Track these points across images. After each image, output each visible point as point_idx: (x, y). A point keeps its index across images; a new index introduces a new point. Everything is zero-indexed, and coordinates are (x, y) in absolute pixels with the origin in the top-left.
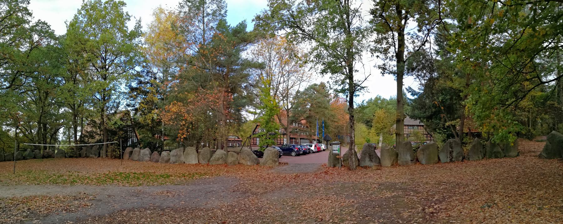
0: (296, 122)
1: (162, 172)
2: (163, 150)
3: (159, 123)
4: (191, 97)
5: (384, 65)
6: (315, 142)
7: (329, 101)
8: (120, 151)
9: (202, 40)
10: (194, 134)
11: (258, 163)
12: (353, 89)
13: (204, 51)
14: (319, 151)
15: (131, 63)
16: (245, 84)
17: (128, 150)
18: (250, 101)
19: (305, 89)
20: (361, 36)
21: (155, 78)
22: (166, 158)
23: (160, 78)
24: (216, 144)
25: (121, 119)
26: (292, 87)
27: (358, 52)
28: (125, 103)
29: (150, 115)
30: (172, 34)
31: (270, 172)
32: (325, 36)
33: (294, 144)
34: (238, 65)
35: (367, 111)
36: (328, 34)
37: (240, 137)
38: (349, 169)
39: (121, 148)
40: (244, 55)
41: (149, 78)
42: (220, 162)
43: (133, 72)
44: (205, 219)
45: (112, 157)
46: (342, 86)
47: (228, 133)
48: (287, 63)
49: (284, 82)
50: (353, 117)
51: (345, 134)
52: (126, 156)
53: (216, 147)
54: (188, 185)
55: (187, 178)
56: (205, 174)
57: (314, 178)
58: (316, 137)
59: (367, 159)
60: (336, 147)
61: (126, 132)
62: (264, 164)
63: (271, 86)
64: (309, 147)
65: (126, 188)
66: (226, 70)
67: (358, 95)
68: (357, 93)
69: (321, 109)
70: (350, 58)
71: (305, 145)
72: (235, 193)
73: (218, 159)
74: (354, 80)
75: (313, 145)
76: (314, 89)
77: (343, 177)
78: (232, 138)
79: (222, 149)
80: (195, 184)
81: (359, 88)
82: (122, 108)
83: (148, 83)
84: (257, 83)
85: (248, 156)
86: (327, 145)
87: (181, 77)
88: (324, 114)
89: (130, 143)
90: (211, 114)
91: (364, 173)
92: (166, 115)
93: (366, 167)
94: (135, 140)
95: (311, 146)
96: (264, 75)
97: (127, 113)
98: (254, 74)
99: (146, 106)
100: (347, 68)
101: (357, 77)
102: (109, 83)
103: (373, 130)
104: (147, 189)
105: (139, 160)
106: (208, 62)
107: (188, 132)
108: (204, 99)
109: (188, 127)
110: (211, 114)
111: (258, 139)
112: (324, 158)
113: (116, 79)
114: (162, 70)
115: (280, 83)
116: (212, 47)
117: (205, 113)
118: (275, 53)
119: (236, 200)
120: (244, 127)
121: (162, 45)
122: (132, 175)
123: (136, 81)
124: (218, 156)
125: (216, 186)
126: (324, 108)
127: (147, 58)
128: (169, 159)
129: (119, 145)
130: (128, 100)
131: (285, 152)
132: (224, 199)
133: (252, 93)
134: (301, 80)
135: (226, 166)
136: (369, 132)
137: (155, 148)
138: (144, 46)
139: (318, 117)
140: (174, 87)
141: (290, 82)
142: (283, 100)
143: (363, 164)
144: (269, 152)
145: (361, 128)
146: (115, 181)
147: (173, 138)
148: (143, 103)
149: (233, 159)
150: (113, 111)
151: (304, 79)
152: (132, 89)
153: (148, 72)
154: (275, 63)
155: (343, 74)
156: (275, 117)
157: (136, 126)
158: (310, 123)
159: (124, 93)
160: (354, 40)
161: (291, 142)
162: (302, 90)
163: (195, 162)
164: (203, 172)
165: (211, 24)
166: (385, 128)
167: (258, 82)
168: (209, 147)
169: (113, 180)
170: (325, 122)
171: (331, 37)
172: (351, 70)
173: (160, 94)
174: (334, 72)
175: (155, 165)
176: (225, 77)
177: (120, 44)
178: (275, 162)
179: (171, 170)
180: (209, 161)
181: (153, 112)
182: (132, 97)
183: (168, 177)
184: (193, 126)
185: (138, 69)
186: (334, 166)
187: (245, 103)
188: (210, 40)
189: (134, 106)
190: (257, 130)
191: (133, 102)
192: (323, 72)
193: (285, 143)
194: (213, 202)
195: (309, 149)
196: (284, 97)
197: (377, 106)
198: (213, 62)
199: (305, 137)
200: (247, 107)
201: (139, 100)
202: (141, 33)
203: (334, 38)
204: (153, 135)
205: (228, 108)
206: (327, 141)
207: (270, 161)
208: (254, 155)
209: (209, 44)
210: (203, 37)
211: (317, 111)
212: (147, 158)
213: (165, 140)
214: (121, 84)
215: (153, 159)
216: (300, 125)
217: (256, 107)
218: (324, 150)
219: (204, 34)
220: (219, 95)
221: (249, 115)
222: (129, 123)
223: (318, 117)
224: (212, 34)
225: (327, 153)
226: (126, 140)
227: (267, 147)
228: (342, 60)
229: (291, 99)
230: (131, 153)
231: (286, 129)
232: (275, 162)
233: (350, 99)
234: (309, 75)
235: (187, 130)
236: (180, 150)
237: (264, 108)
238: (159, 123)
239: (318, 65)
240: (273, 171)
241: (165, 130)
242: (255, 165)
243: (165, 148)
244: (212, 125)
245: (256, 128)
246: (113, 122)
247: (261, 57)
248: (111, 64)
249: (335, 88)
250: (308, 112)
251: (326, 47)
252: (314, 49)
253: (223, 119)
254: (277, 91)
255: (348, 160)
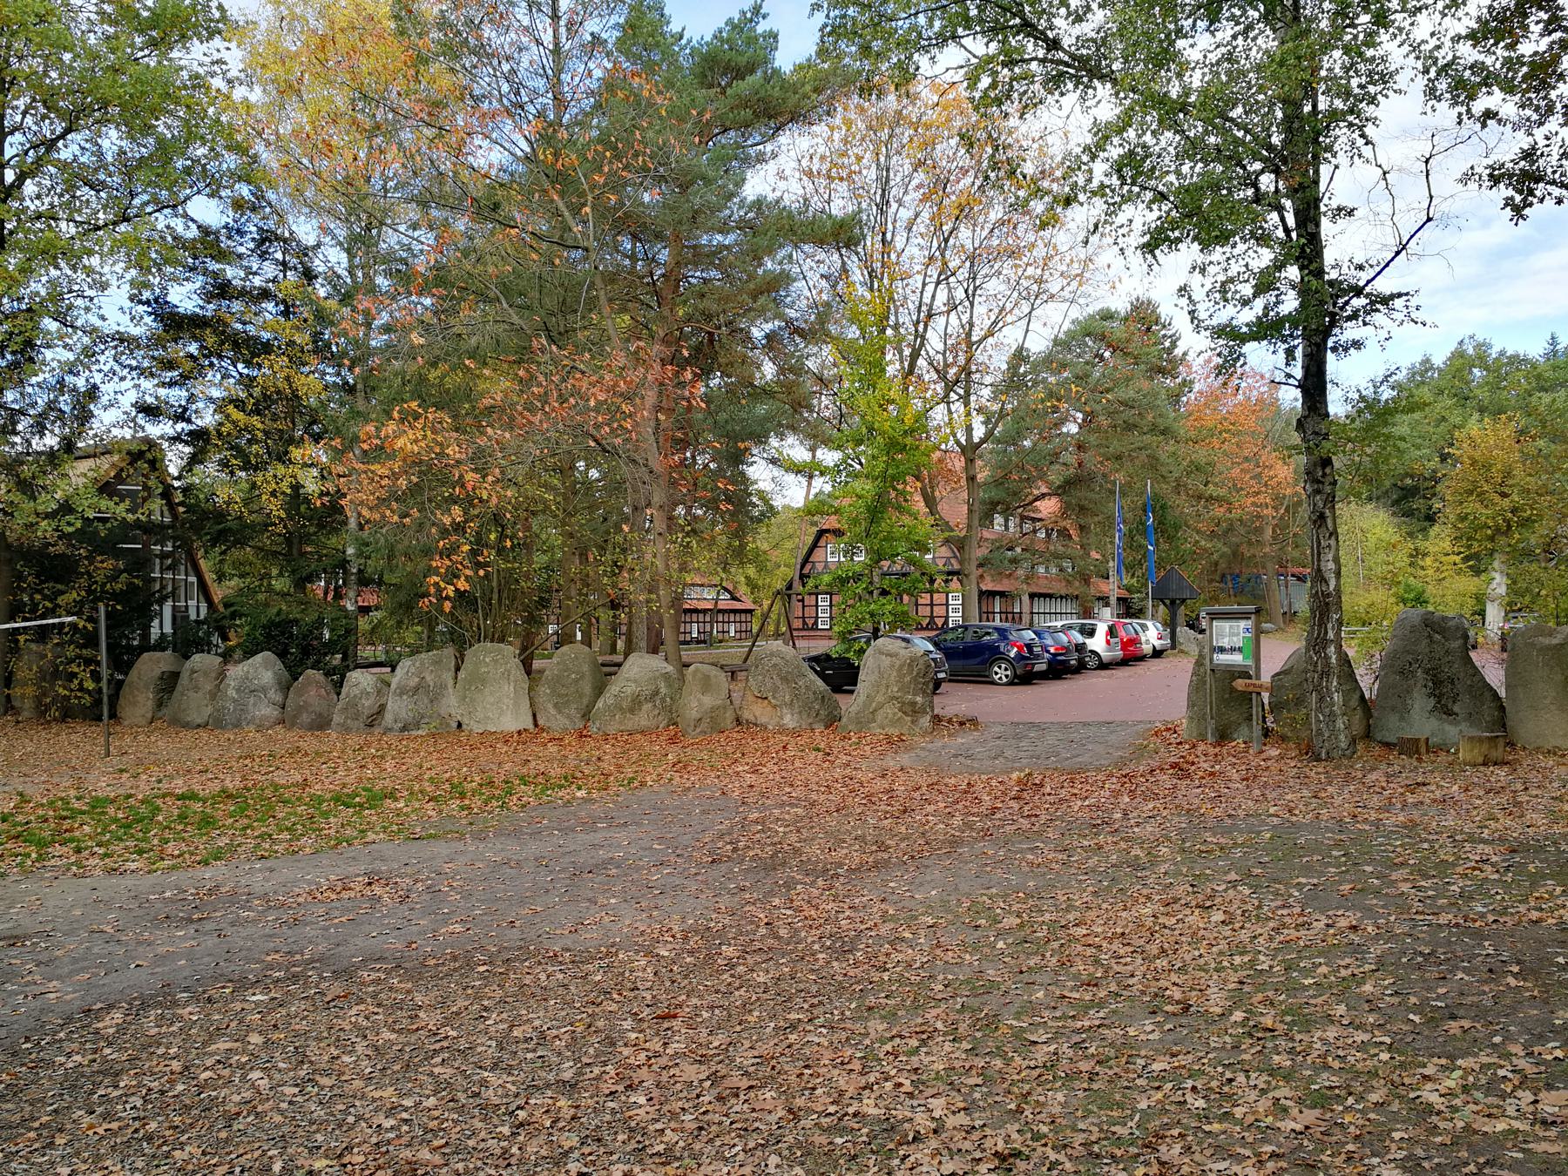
0: (1007, 513)
1: (347, 776)
2: (351, 662)
3: (330, 515)
4: (496, 387)
5: (1529, 155)
6: (1107, 613)
7: (1175, 397)
8: (96, 677)
9: (548, 100)
10: (508, 579)
11: (832, 720)
12: (1322, 313)
13: (556, 155)
14: (1131, 656)
15: (162, 172)
16: (768, 327)
17: (151, 666)
18: (791, 405)
19: (1056, 342)
20: (1365, 18)
21: (309, 275)
22: (368, 704)
23: (333, 278)
24: (620, 627)
25: (106, 489)
26: (990, 333)
27: (1355, 110)
28: (132, 396)
29: (281, 470)
30: (393, 54)
31: (891, 762)
32: (1165, 57)
33: (997, 623)
34: (724, 230)
35: (1402, 426)
36: (1180, 44)
37: (743, 590)
38: (1311, 753)
39: (103, 656)
40: (757, 184)
41: (270, 270)
42: (644, 718)
43: (178, 225)
44: (571, 1004)
45: (41, 711)
46: (1259, 304)
47: (683, 568)
48: (964, 212)
49: (952, 306)
50: (1326, 462)
51: (1272, 567)
52: (139, 701)
53: (620, 644)
54: (480, 837)
55: (477, 802)
56: (570, 779)
57: (1116, 794)
58: (1112, 588)
59: (1420, 703)
60: (1231, 634)
61: (139, 563)
62: (862, 722)
63: (889, 332)
64: (1079, 638)
65: (129, 881)
66: (664, 255)
67: (1357, 344)
68: (1351, 331)
69: (1136, 439)
70: (1301, 149)
71: (1057, 628)
72: (723, 867)
73: (636, 703)
74: (1329, 257)
75: (1102, 629)
76: (1102, 338)
77: (1271, 793)
78: (703, 597)
79: (654, 650)
80: (516, 833)
81: (1359, 302)
82: (111, 420)
83: (265, 294)
84: (823, 318)
85: (785, 679)
86: (1171, 625)
87: (440, 278)
88: (1153, 464)
89: (161, 626)
90: (594, 474)
91: (1404, 779)
92: (357, 476)
93: (1411, 748)
94: (196, 609)
95: (1091, 633)
96: (857, 275)
97: (145, 455)
98: (810, 275)
99: (255, 421)
100: (1288, 204)
101: (1342, 247)
102: (26, 271)
103: (1440, 540)
104: (257, 878)
105: (216, 723)
106: (576, 210)
107: (479, 565)
108: (562, 400)
109: (480, 542)
110: (594, 474)
111: (824, 602)
112: (1164, 693)
113: (73, 256)
114: (342, 233)
115: (930, 316)
116: (600, 141)
117: (565, 470)
118: (908, 168)
119: (725, 902)
120: (760, 541)
121: (341, 101)
122: (172, 808)
123: (199, 281)
124: (631, 689)
125: (622, 836)
126: (1154, 429)
127: (255, 159)
128: (382, 708)
129: (91, 640)
130: (147, 384)
131: (959, 663)
132: (665, 902)
133: (799, 370)
134: (1038, 294)
135: (673, 740)
136: (1417, 553)
137: (308, 649)
138: (239, 93)
139: (1120, 477)
140: (407, 330)
141: (980, 309)
142: (945, 399)
143: (1392, 728)
144: (887, 661)
145: (1367, 526)
146: (58, 850)
147: (402, 596)
148: (239, 404)
149: (708, 701)
150: (51, 441)
151: (1054, 286)
152: (174, 324)
153: (266, 238)
154: (905, 214)
155: (1264, 239)
156: (912, 486)
157: (197, 528)
158: (1082, 509)
159: (122, 338)
160: (1326, 48)
161: (987, 614)
162: (1038, 344)
163: (513, 719)
164: (556, 771)
165: (592, 26)
166: (1526, 523)
167: (824, 313)
168: (587, 641)
169: (42, 844)
170: (1158, 506)
171: (1194, 55)
172: (1309, 215)
173: (336, 360)
174: (1212, 235)
175: (309, 743)
176: (667, 289)
177: (94, 56)
178: (914, 711)
179: (389, 765)
180: (586, 715)
181: (296, 453)
182: (170, 365)
183: (376, 799)
184: (499, 530)
185: (207, 211)
186: (1223, 737)
187: (768, 418)
188: (588, 103)
189: (181, 416)
190: (818, 555)
191: (177, 396)
192: (1156, 241)
193: (955, 618)
194: (616, 919)
195: (1080, 648)
196: (949, 388)
197: (1464, 399)
198: (601, 211)
199: (1059, 588)
200: (774, 442)
201: (216, 385)
202: (224, 18)
203: (1213, 57)
204: (302, 582)
205: (683, 444)
206: (1176, 605)
207: (891, 710)
208: (813, 676)
209: (581, 122)
210: (555, 85)
211: (1115, 446)
212: (266, 711)
213: (365, 610)
214: (104, 286)
215: (300, 709)
216: (1027, 527)
217: (816, 438)
218: (1157, 653)
219: (558, 71)
220: (635, 375)
221: (784, 479)
222: (156, 510)
223: (1120, 477)
224: (598, 73)
225: (1177, 675)
226: (134, 607)
227: (876, 634)
228: (1258, 166)
229: (986, 392)
230: (170, 682)
231: (960, 545)
232: (914, 711)
233: (1306, 368)
234: (1076, 269)
235: (474, 553)
236: (437, 662)
237: (859, 442)
238: (330, 515)
239: (1128, 211)
240: (905, 759)
241: (359, 554)
242: (819, 728)
243: (366, 652)
244: (600, 528)
245: (815, 545)
246: (46, 503)
247: (842, 188)
248: (39, 162)
249: (1222, 317)
250: (1070, 457)
251: (1171, 112)
252: (1103, 135)
253: (657, 498)
254: (915, 355)
255: (1299, 702)
